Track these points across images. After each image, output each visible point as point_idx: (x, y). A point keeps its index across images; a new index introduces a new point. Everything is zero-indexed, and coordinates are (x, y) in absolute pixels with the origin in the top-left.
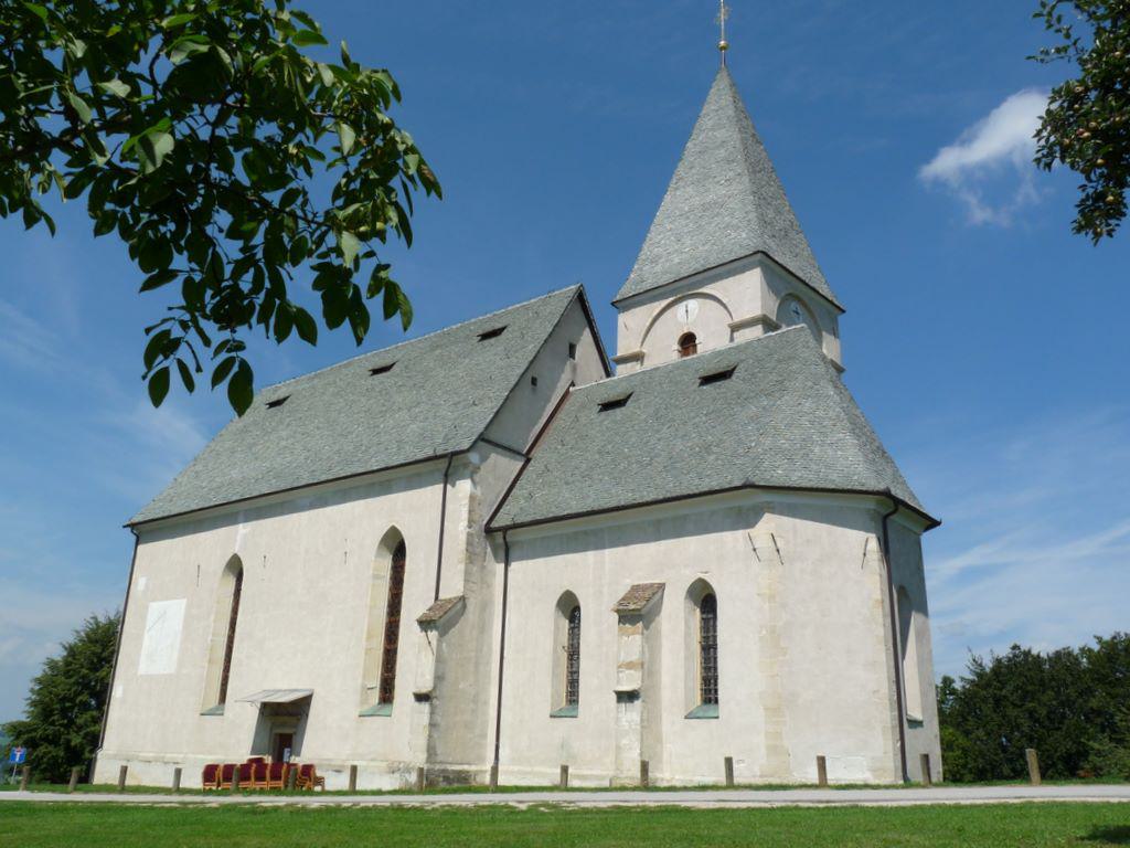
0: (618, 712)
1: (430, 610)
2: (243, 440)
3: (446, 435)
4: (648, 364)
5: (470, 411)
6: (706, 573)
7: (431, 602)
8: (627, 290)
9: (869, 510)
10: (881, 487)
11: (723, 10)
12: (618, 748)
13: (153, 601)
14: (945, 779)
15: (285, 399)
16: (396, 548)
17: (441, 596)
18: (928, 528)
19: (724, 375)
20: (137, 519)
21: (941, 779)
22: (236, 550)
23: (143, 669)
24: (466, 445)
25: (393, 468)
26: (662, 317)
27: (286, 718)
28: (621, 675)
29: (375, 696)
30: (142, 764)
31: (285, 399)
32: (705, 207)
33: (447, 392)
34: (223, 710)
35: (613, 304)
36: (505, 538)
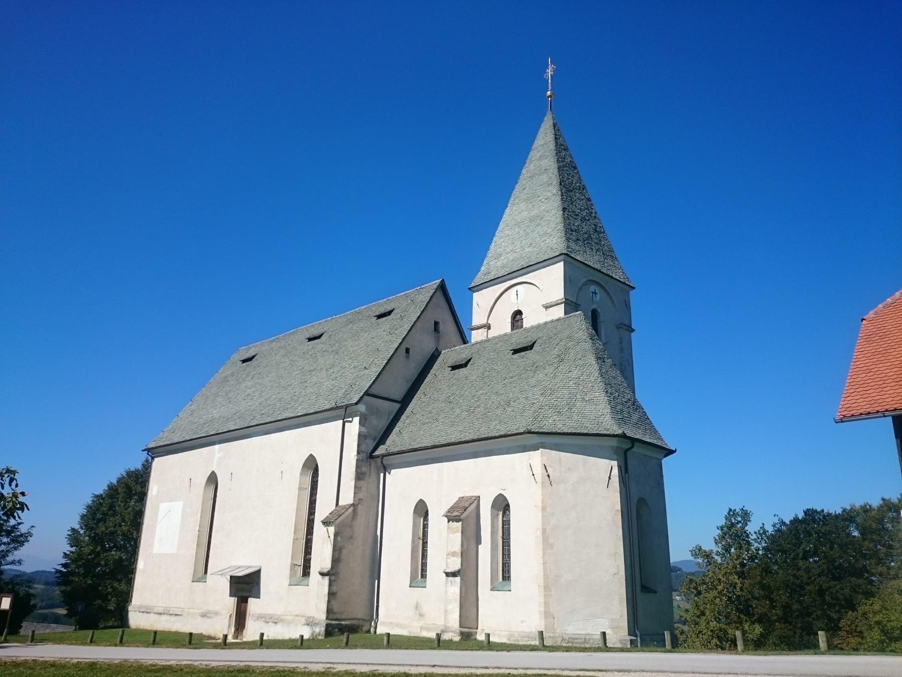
0: (446, 586)
1: (330, 514)
2: (223, 388)
3: (346, 391)
4: (493, 333)
5: (362, 373)
6: (505, 490)
7: (333, 507)
8: (478, 280)
9: (613, 447)
10: (620, 432)
11: (550, 67)
12: (446, 611)
13: (162, 502)
14: (829, 649)
15: (253, 357)
16: (312, 466)
17: (340, 504)
18: (666, 456)
19: (530, 347)
20: (151, 445)
21: (827, 649)
22: (214, 469)
23: (156, 550)
24: (355, 400)
25: (311, 414)
26: (509, 291)
27: (244, 586)
28: (448, 560)
29: (300, 571)
30: (157, 616)
31: (253, 357)
32: (532, 220)
33: (351, 358)
34: (206, 578)
35: (469, 289)
36: (382, 462)
